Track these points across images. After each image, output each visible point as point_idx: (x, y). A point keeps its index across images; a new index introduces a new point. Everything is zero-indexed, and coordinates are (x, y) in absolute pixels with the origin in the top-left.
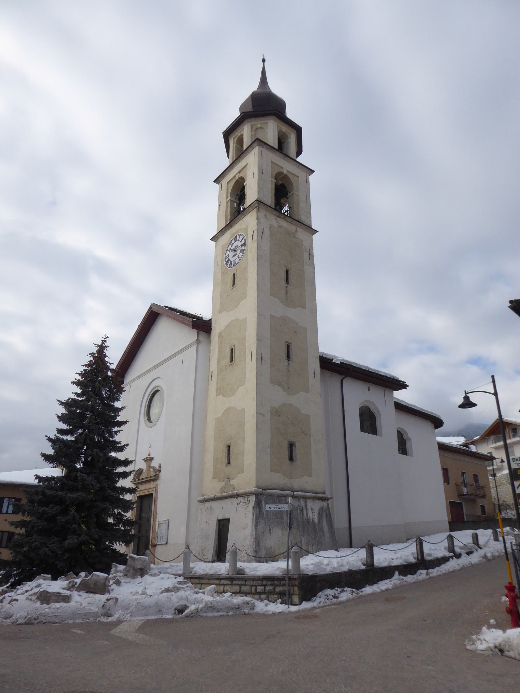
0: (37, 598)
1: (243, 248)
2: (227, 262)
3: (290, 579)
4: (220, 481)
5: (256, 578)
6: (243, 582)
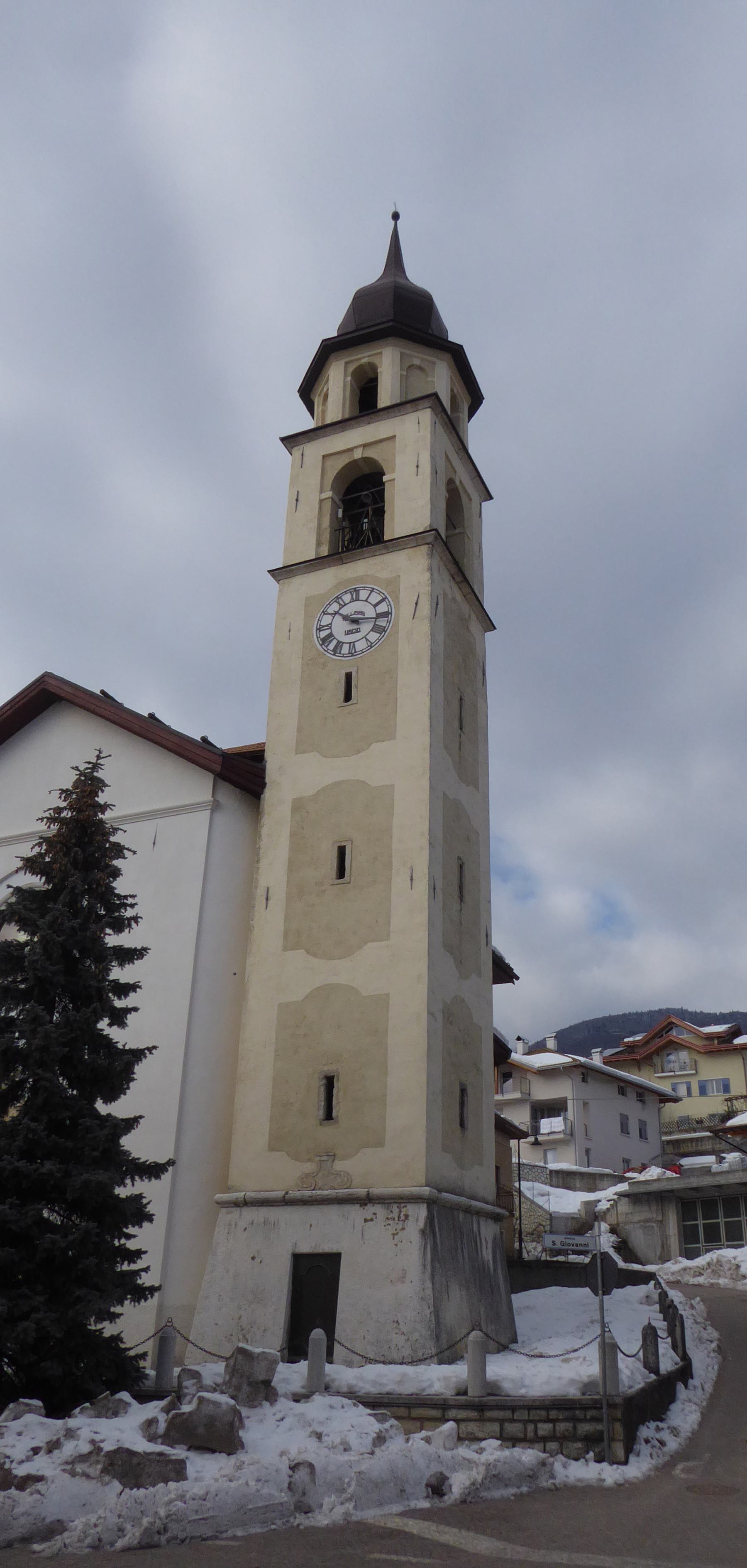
0: (104, 1471)
1: (382, 622)
2: (324, 641)
3: (612, 1406)
4: (296, 1157)
5: (537, 1403)
6: (508, 1414)
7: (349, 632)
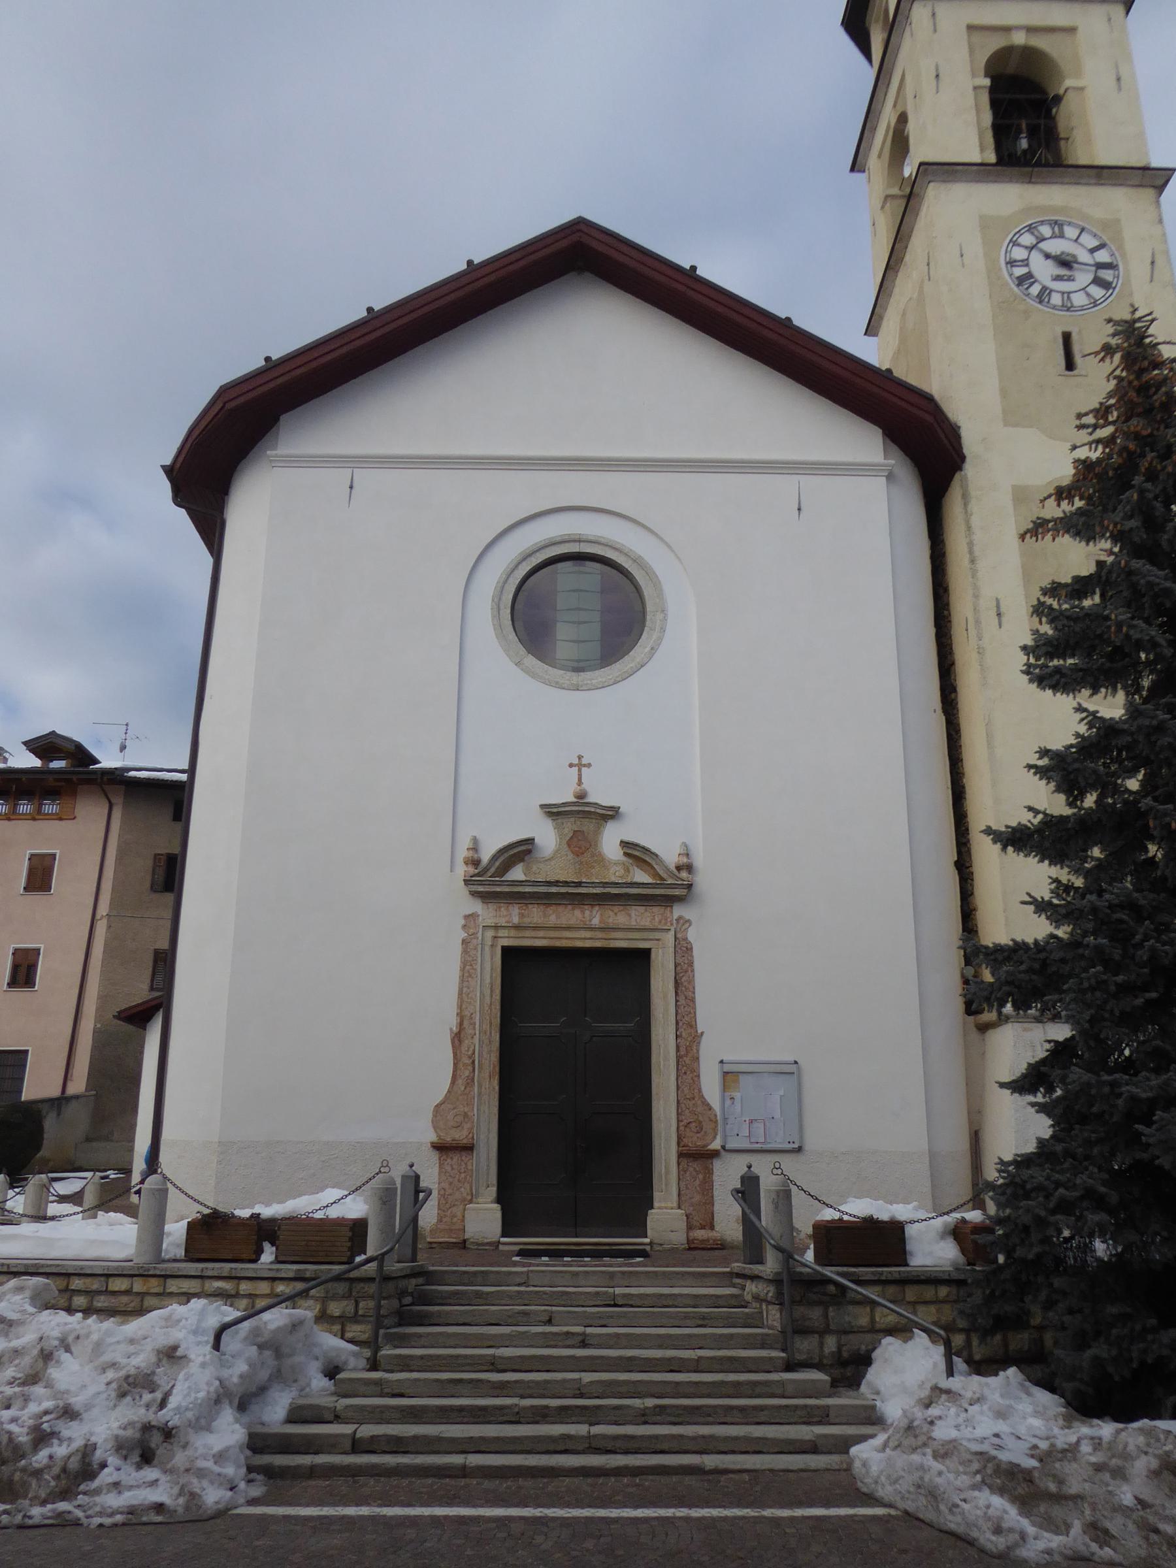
1: (1107, 275)
2: (1021, 280)
6: (154, 1285)
7: (1058, 278)
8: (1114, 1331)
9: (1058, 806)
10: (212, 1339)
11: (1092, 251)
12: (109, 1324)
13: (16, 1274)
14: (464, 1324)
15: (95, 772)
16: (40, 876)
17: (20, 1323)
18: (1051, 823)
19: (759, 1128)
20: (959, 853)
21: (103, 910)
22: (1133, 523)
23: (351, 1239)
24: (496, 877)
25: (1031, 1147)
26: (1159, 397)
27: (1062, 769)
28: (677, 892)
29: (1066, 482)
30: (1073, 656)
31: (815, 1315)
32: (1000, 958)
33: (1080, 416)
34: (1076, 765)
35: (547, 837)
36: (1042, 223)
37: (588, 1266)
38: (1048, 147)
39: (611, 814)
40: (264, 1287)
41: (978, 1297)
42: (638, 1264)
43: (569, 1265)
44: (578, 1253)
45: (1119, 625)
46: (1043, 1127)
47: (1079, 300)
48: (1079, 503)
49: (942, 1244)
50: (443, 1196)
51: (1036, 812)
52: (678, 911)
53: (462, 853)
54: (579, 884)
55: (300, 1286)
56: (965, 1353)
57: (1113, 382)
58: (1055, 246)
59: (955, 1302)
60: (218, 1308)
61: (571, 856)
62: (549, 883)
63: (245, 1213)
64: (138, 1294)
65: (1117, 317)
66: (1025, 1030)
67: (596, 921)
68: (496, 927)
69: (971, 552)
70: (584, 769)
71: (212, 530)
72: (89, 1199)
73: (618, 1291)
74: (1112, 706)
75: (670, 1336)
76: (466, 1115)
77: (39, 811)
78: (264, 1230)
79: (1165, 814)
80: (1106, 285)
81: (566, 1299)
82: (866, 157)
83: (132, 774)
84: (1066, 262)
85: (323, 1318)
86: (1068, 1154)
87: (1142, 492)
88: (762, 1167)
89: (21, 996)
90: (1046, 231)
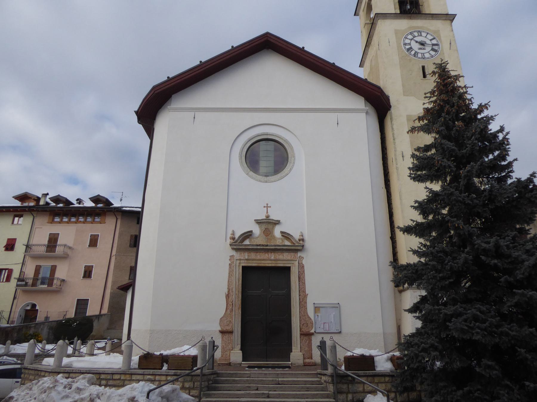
1: (436, 48)
2: (408, 50)
6: (128, 377)
7: (420, 49)
8: (442, 391)
9: (420, 219)
10: (146, 395)
11: (431, 40)
12: (113, 390)
13: (83, 373)
14: (229, 390)
15: (112, 208)
16: (94, 242)
17: (84, 389)
18: (418, 224)
19: (327, 326)
20: (392, 234)
21: (114, 253)
22: (443, 128)
23: (192, 362)
24: (240, 243)
25: (414, 331)
26: (450, 88)
27: (422, 207)
28: (299, 248)
29: (421, 115)
30: (425, 170)
31: (345, 387)
32: (402, 269)
33: (425, 94)
34: (426, 206)
35: (257, 230)
36: (415, 31)
37: (270, 371)
38: (416, 8)
39: (277, 223)
40: (163, 378)
41: (399, 380)
42: (287, 371)
43: (264, 371)
44: (267, 367)
45: (438, 161)
46: (419, 324)
47: (427, 55)
48: (426, 122)
49: (387, 363)
50: (223, 348)
51: (414, 221)
52: (299, 254)
53: (229, 235)
54: (267, 245)
55: (175, 377)
56: (395, 400)
57: (436, 83)
58: (419, 39)
59: (391, 382)
60: (148, 385)
61: (264, 236)
62: (257, 245)
63: (158, 353)
64: (123, 380)
65: (437, 62)
66: (414, 292)
67: (273, 258)
68: (240, 260)
69: (393, 137)
70: (269, 208)
71: (150, 132)
72: (108, 349)
73: (280, 379)
74: (436, 187)
75: (297, 394)
76: (230, 321)
77: (94, 221)
78: (164, 359)
79: (454, 222)
80: (436, 51)
81: (262, 382)
82: (359, 11)
83: (124, 208)
84: (422, 44)
85: (183, 388)
86: (426, 332)
87: (445, 118)
88: (327, 338)
89: (87, 281)
90: (416, 34)
